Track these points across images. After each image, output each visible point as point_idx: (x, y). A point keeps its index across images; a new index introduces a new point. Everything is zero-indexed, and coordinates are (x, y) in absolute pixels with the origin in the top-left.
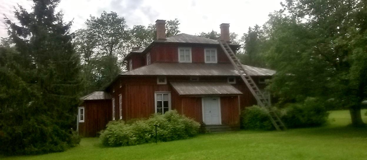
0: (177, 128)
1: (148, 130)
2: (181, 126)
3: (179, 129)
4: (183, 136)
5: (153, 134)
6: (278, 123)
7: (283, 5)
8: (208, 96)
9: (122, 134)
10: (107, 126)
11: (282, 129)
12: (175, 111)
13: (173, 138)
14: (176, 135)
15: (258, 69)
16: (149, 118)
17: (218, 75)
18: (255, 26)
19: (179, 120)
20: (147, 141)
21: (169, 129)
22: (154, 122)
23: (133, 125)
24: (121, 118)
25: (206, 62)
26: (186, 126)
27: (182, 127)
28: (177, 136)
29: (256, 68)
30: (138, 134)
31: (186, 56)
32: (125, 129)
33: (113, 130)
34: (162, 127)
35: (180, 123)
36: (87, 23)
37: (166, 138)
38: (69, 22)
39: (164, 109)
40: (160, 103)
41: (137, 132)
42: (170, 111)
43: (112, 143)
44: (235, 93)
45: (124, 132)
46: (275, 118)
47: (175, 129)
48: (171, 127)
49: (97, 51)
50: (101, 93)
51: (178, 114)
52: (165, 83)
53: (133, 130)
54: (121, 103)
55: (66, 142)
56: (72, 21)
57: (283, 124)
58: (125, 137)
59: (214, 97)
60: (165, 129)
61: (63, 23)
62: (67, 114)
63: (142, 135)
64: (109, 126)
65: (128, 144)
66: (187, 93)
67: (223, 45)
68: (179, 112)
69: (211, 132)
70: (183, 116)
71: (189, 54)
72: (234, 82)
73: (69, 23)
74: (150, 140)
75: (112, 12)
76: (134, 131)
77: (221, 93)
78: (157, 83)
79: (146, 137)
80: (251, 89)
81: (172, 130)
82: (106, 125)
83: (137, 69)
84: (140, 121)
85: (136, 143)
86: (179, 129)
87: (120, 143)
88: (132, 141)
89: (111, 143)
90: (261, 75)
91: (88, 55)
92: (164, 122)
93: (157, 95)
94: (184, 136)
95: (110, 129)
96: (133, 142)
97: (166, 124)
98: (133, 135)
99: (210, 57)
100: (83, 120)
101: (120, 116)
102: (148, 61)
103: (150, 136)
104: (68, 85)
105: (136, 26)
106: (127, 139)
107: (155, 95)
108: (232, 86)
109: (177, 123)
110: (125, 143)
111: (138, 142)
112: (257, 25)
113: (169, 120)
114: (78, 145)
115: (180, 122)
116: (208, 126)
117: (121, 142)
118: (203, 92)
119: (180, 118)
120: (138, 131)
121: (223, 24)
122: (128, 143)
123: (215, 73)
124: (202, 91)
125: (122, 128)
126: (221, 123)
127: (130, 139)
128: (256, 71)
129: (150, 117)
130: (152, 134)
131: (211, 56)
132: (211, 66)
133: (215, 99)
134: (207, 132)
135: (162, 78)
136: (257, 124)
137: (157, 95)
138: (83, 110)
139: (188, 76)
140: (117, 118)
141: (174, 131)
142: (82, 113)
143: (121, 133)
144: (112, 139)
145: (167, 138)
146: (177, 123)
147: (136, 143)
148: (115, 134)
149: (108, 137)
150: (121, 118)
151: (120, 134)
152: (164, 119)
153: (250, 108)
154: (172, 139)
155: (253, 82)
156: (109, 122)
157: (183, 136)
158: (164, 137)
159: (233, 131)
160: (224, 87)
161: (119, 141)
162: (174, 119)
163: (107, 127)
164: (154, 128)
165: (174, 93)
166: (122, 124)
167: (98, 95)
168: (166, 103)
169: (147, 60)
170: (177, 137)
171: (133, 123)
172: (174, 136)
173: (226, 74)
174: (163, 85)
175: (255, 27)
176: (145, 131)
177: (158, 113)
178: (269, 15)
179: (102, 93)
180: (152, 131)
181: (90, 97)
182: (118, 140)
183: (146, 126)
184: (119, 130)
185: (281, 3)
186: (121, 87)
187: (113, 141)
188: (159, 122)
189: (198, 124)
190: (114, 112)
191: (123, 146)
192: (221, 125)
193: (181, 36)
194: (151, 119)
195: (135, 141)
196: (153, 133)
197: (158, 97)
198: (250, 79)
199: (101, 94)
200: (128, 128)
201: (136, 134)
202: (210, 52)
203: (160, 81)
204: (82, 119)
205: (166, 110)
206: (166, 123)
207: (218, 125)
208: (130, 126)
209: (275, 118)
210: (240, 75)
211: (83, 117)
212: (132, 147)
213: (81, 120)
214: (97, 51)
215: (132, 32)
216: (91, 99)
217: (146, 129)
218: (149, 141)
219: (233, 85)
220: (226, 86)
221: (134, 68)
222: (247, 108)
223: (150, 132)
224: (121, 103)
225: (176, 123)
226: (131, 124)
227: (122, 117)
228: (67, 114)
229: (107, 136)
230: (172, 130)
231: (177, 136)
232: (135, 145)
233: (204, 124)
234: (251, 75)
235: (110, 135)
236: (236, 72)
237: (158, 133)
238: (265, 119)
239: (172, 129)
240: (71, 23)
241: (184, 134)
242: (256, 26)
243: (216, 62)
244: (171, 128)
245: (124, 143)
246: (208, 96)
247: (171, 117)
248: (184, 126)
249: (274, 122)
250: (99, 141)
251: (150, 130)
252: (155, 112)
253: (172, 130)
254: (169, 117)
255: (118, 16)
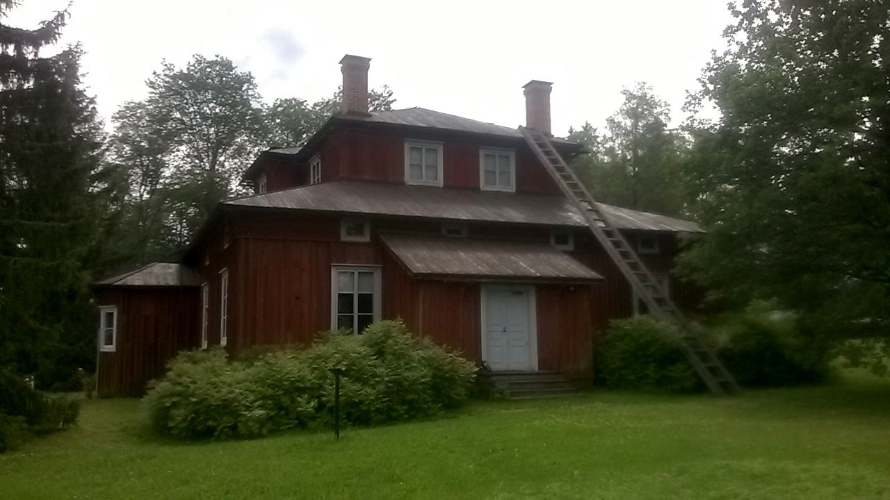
0: (406, 379)
1: (309, 385)
2: (419, 374)
3: (411, 384)
4: (426, 406)
5: (324, 399)
6: (713, 370)
7: (736, 14)
8: (489, 280)
9: (215, 397)
10: (168, 366)
11: (727, 389)
12: (397, 324)
13: (394, 414)
14: (403, 402)
15: (632, 214)
16: (313, 345)
17: (525, 221)
18: (584, 125)
19: (414, 354)
20: (303, 424)
21: (378, 382)
22: (327, 358)
23: (257, 366)
24: (224, 342)
25: (483, 186)
26: (434, 376)
27: (422, 377)
28: (406, 407)
29: (626, 211)
30: (271, 397)
31: (426, 166)
32: (229, 380)
33: (186, 380)
34: (354, 372)
35: (414, 364)
36: (151, 83)
37: (367, 412)
38: (56, 14)
39: (359, 316)
40: (346, 300)
41: (270, 392)
42: (378, 326)
43: (181, 426)
44: (581, 276)
45: (224, 391)
46: (704, 357)
47: (398, 383)
48: (387, 376)
49: (177, 160)
50: (171, 268)
51: (409, 335)
52: (366, 239)
53: (256, 383)
54: (224, 297)
55: (22, 418)
56: (66, 11)
57: (728, 377)
58: (225, 407)
59: (519, 284)
60: (365, 383)
61: (79, 74)
62: (33, 324)
63: (286, 401)
64: (175, 368)
65: (235, 433)
66: (436, 268)
67: (535, 140)
68: (411, 327)
69: (512, 394)
70: (427, 341)
71: (437, 162)
72: (570, 247)
73: (56, 18)
74: (313, 418)
75: (217, 56)
76: (260, 389)
77: (538, 275)
78: (339, 236)
79: (299, 409)
80: (623, 266)
81: (389, 388)
82: (167, 363)
83: (280, 192)
84: (279, 354)
85: (265, 431)
86: (414, 382)
87: (208, 426)
88: (251, 424)
89: (176, 427)
90: (647, 229)
91: (152, 175)
92: (364, 357)
93: (411, 148)
94: (429, 408)
95: (179, 376)
96: (255, 427)
97: (369, 366)
98: (255, 401)
99: (494, 172)
100: (112, 344)
101: (222, 335)
102: (315, 175)
103: (312, 404)
104: (41, 224)
105: (281, 101)
106: (235, 414)
107: (334, 272)
108: (566, 257)
109: (406, 364)
110: (224, 427)
111: (269, 426)
112: (588, 124)
113: (380, 353)
114: (71, 426)
115: (416, 359)
116: (499, 374)
117: (210, 423)
118: (482, 269)
119: (415, 346)
120: (273, 389)
121: (533, 82)
122: (234, 427)
123: (515, 215)
124: (482, 266)
125: (217, 376)
126: (536, 368)
127: (244, 415)
128: (624, 215)
129: (316, 340)
130: (319, 397)
131: (497, 172)
132: (497, 198)
133: (519, 293)
134: (498, 395)
135: (358, 221)
136: (648, 372)
137: (339, 272)
138: (112, 314)
139: (437, 219)
140: (214, 339)
141: (395, 389)
142: (110, 323)
143: (213, 392)
144: (179, 414)
145: (373, 414)
146: (406, 364)
147: (265, 431)
148: (193, 395)
149: (168, 405)
150: (224, 342)
151: (207, 395)
152: (361, 349)
153: (624, 324)
154: (388, 417)
155: (627, 247)
156: (177, 354)
157: (426, 406)
158: (364, 408)
159: (577, 391)
160: (542, 256)
161: (206, 420)
162: (395, 350)
163: (170, 370)
164: (326, 378)
165: (395, 272)
166: (218, 359)
167: (163, 274)
168: (366, 301)
169: (310, 177)
170: (406, 413)
171: (259, 360)
172: (398, 407)
173: (544, 220)
174: (358, 244)
175: (583, 127)
176: (296, 389)
177: (343, 328)
178: (624, 93)
179: (173, 267)
180: (321, 387)
181: (136, 279)
182: (202, 418)
183: (298, 372)
184: (208, 383)
185: (731, 6)
186: (226, 246)
187: (184, 420)
188: (345, 358)
189: (471, 368)
190: (205, 324)
191: (218, 439)
192: (537, 374)
193: (414, 112)
194: (319, 349)
195: (261, 422)
196: (324, 396)
197: (341, 282)
198: (620, 238)
199: (171, 271)
200: (241, 375)
201: (264, 397)
202: (497, 158)
203: (349, 233)
204: (109, 342)
205: (365, 322)
206: (370, 363)
207: (531, 374)
208: (248, 371)
209: (704, 357)
210: (587, 225)
211: (112, 334)
212: (247, 448)
213: (107, 344)
214: (177, 160)
215: (274, 114)
216: (137, 283)
217: (302, 379)
218: (311, 424)
219: (566, 252)
220: (550, 256)
221: (270, 189)
222: (613, 322)
223: (314, 391)
224: (224, 297)
225: (402, 363)
226: (249, 362)
227: (226, 338)
228: (33, 324)
229: (164, 400)
230: (391, 385)
231: (406, 407)
232: (260, 436)
233: (485, 368)
234: (622, 227)
235: (174, 399)
236: (575, 217)
237: (341, 395)
238: (670, 356)
239: (389, 382)
240: (63, 19)
241: (429, 399)
242: (586, 127)
243: (512, 189)
244: (386, 379)
245: (219, 428)
246: (489, 280)
247: (384, 342)
248: (431, 374)
249: (700, 367)
250: (141, 412)
251: (312, 383)
252: (330, 329)
253: (391, 385)
254: (378, 344)
255: (236, 69)
